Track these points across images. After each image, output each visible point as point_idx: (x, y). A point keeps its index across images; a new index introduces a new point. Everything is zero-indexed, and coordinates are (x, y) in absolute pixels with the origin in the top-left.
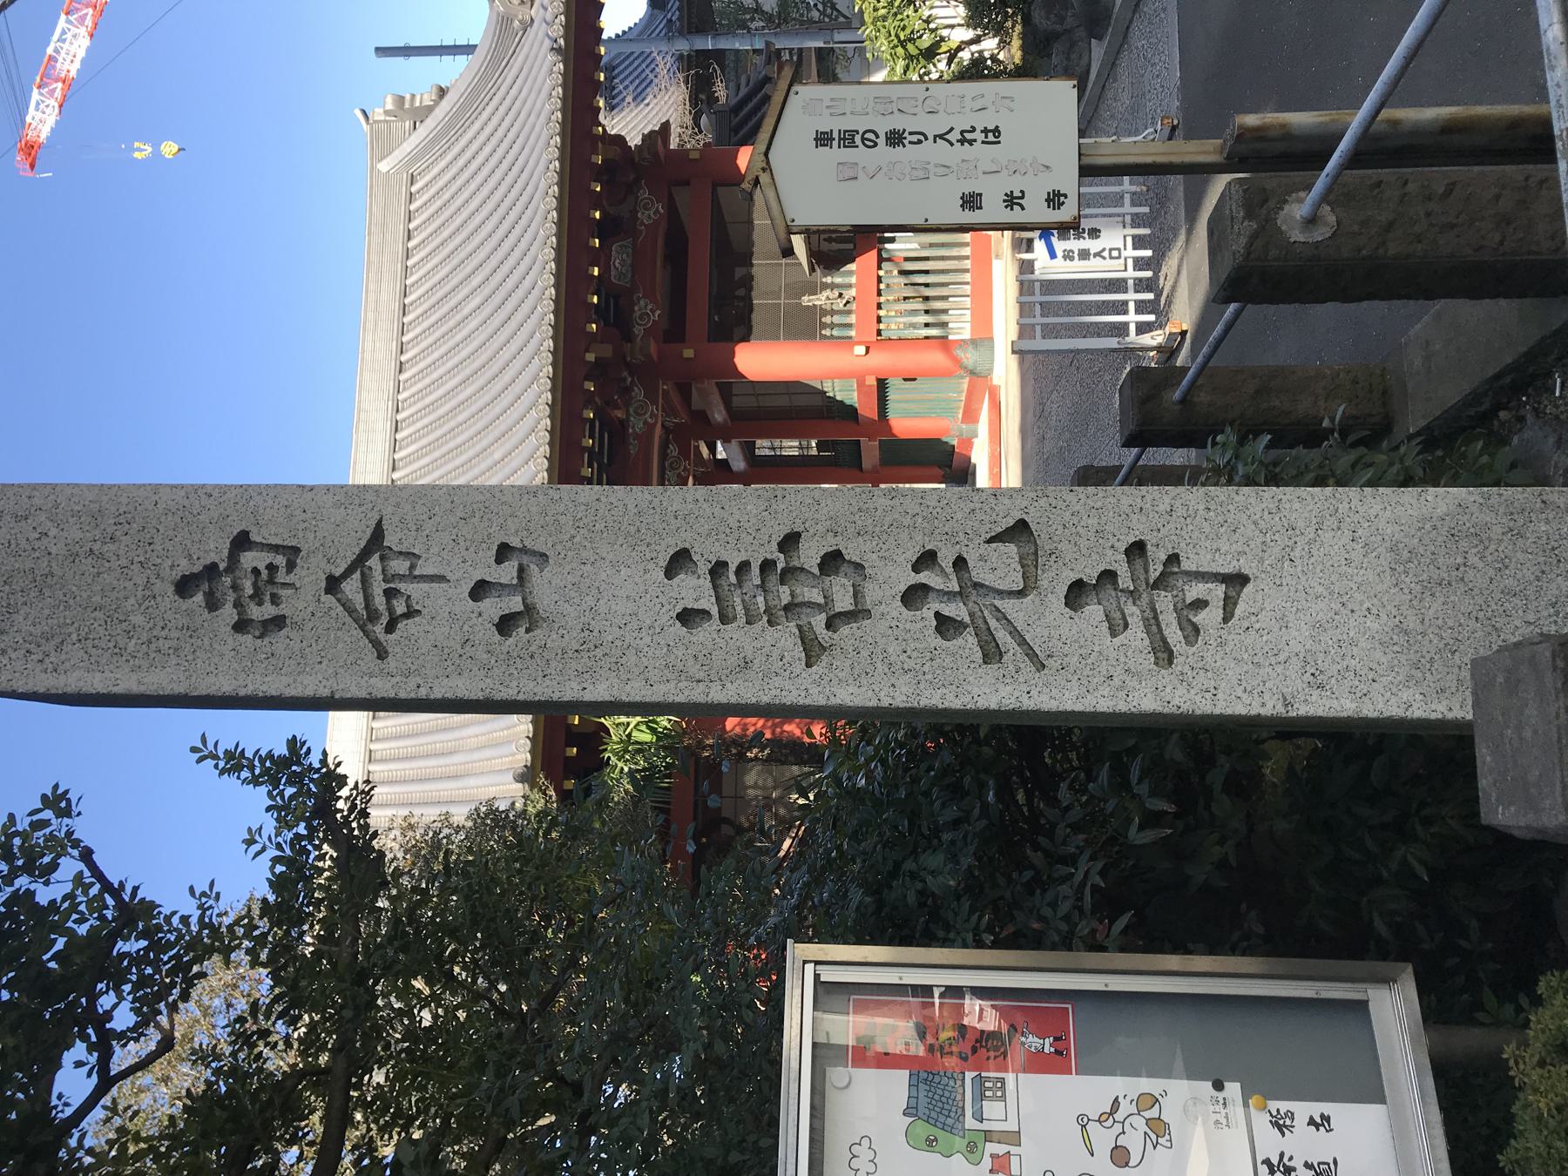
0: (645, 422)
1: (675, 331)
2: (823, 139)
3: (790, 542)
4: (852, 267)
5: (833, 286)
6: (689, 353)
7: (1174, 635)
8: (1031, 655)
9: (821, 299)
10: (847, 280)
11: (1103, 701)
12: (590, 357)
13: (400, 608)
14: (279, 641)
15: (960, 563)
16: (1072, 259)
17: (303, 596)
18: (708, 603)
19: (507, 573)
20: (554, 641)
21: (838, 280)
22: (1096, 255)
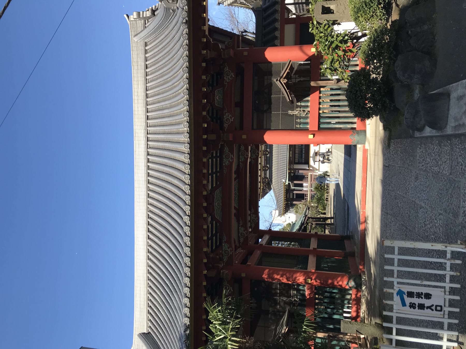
0: (229, 161)
4: (309, 98)
5: (301, 107)
9: (296, 112)
10: (306, 104)
16: (414, 308)
21: (303, 104)
22: (428, 308)
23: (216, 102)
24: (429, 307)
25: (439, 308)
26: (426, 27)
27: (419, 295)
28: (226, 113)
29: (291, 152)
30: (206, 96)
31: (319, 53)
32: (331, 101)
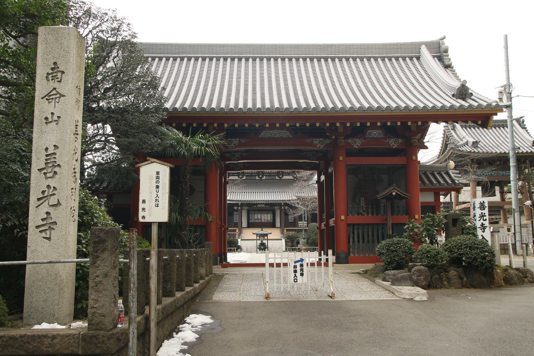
0: (317, 144)
1: (351, 153)
2: (158, 173)
3: (59, 166)
6: (341, 158)
7: (41, 229)
8: (38, 206)
11: (31, 217)
12: (338, 124)
13: (50, 101)
14: (45, 81)
15: (54, 194)
17: (53, 84)
18: (49, 152)
19: (55, 118)
20: (43, 127)
22: (295, 275)
23: (371, 131)
24: (295, 275)
25: (296, 280)
26: (445, 283)
27: (302, 270)
28: (361, 140)
29: (263, 206)
30: (221, 125)
31: (451, 203)
32: (359, 242)
